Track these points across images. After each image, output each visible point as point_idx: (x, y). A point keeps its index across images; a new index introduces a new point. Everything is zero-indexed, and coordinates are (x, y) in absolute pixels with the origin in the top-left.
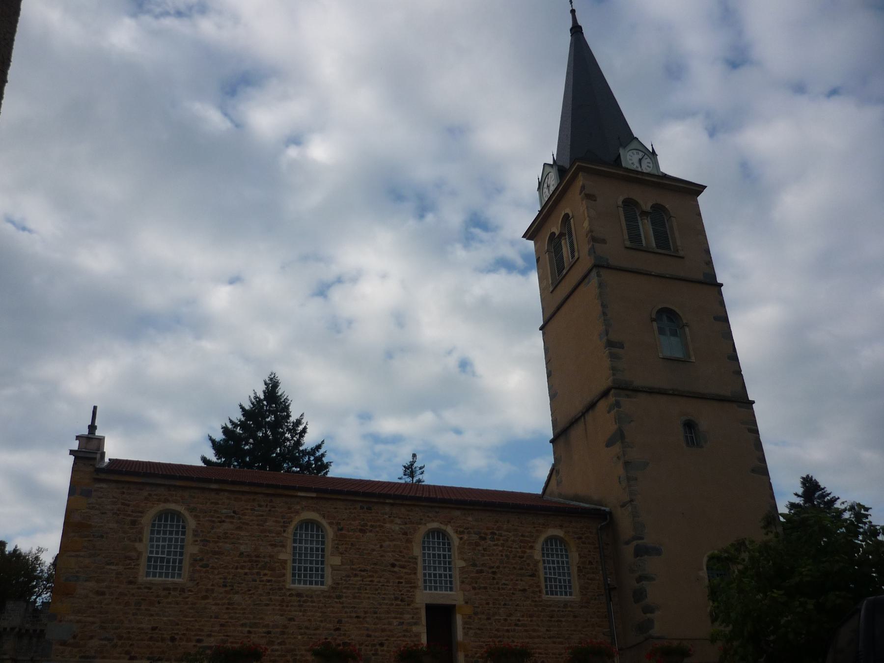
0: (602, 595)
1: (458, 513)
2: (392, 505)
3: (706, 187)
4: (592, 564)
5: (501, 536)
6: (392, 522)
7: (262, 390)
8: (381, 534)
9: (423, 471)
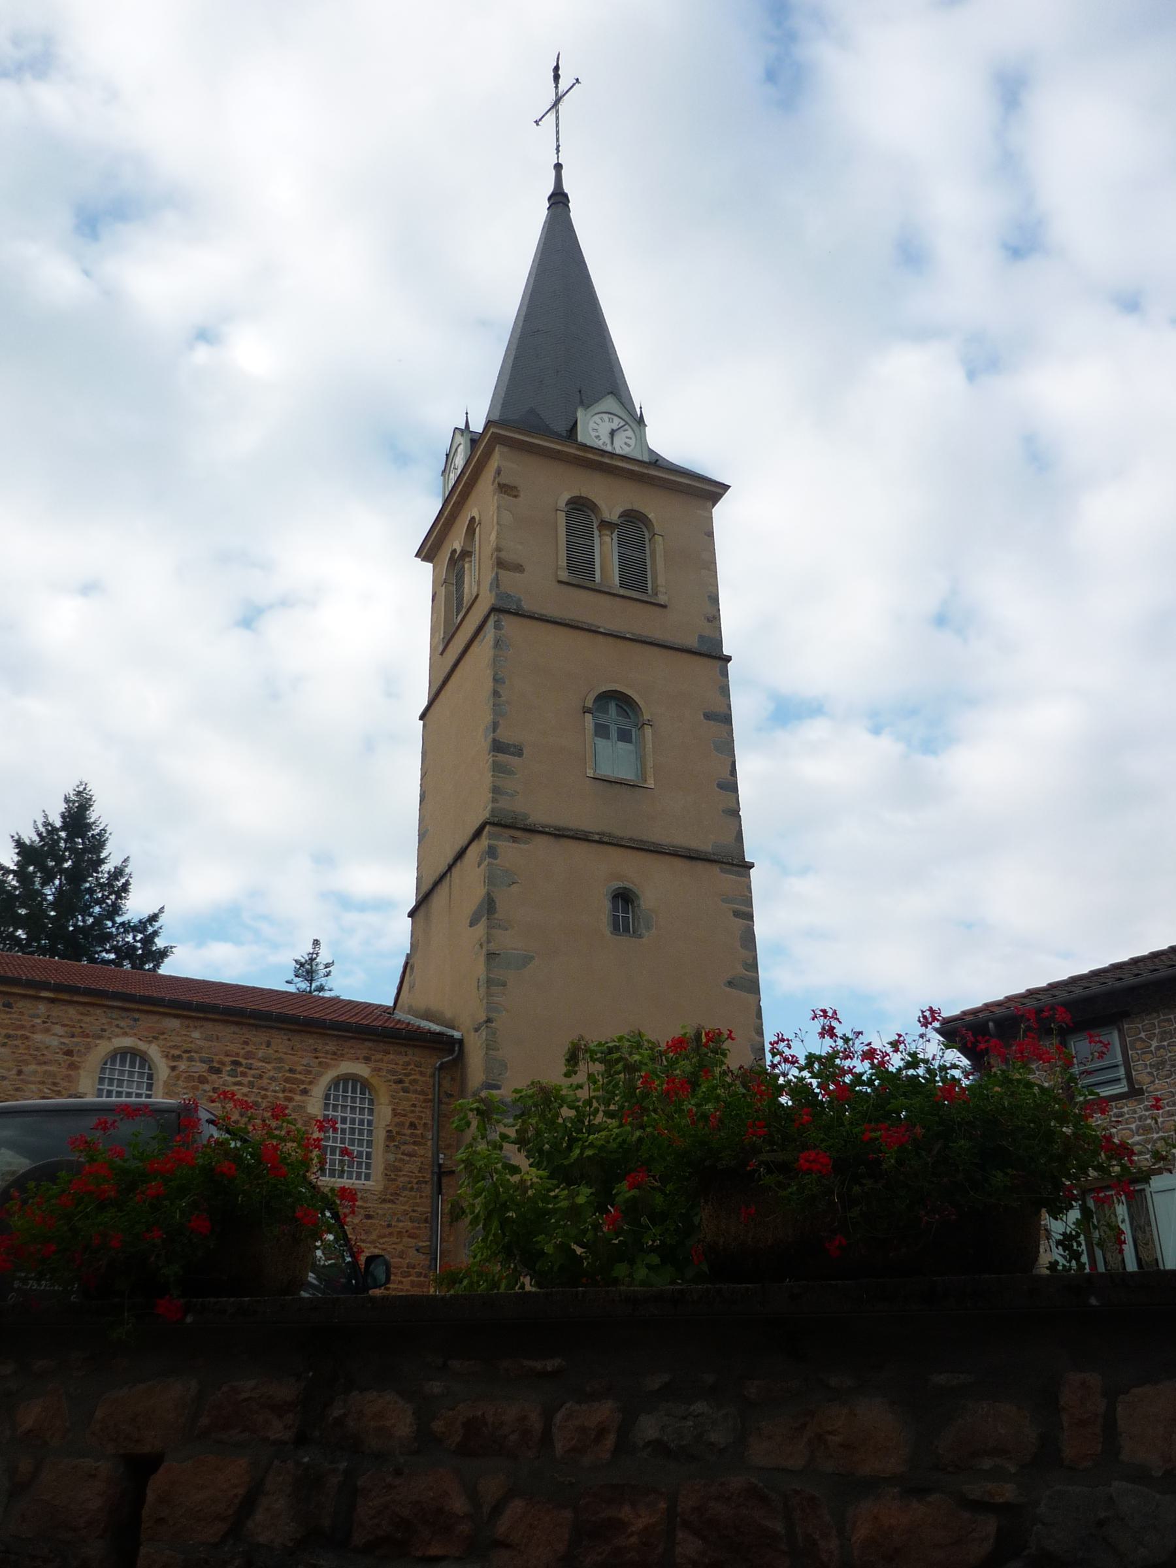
0: (426, 1182)
1: (175, 1023)
2: (52, 1001)
3: (729, 487)
4: (416, 1128)
5: (250, 1069)
6: (47, 1031)
7: (60, 811)
8: (23, 1052)
9: (330, 971)
